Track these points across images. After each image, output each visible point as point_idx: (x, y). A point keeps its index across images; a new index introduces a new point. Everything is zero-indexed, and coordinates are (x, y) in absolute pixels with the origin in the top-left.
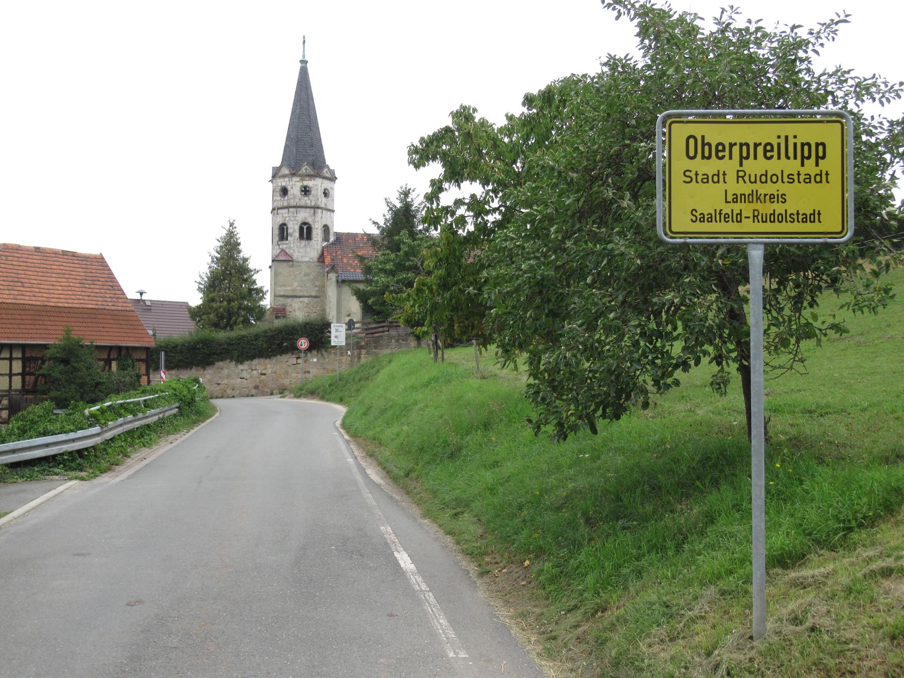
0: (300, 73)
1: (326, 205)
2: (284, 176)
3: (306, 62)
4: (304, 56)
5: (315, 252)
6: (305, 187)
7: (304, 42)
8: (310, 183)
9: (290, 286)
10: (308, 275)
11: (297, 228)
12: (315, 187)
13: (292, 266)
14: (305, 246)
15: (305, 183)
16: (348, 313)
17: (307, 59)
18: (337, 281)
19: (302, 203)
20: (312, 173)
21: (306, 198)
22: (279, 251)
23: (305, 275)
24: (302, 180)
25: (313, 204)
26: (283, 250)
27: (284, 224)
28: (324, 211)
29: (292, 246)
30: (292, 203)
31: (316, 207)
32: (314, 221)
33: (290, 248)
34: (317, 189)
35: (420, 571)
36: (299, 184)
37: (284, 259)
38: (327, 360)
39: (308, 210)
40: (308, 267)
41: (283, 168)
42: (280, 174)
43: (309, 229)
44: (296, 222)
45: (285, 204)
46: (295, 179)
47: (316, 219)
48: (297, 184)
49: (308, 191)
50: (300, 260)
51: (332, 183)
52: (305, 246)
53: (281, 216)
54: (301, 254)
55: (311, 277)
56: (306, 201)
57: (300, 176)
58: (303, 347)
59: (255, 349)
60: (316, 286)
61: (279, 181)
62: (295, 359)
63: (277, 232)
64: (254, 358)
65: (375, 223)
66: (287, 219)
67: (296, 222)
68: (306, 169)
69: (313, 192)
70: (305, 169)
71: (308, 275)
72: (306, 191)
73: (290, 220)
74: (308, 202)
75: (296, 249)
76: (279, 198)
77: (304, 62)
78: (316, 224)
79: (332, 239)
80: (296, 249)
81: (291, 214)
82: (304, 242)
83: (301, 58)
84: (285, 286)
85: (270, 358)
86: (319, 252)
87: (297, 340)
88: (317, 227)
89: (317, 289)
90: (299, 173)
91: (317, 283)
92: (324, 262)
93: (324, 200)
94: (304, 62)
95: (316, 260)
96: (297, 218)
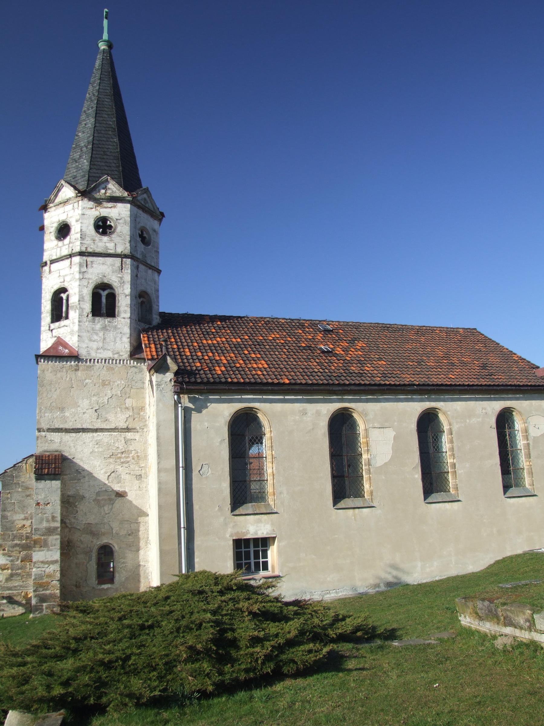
1: (144, 256)
6: (104, 220)
11: (87, 293)
14: (104, 328)
21: (105, 238)
27: (64, 290)
35: (106, 304)
39: (109, 260)
43: (112, 298)
49: (110, 227)
50: (93, 355)
65: (174, 575)
66: (67, 279)
82: (100, 322)
87: (461, 626)
94: (160, 225)
96: (86, 276)
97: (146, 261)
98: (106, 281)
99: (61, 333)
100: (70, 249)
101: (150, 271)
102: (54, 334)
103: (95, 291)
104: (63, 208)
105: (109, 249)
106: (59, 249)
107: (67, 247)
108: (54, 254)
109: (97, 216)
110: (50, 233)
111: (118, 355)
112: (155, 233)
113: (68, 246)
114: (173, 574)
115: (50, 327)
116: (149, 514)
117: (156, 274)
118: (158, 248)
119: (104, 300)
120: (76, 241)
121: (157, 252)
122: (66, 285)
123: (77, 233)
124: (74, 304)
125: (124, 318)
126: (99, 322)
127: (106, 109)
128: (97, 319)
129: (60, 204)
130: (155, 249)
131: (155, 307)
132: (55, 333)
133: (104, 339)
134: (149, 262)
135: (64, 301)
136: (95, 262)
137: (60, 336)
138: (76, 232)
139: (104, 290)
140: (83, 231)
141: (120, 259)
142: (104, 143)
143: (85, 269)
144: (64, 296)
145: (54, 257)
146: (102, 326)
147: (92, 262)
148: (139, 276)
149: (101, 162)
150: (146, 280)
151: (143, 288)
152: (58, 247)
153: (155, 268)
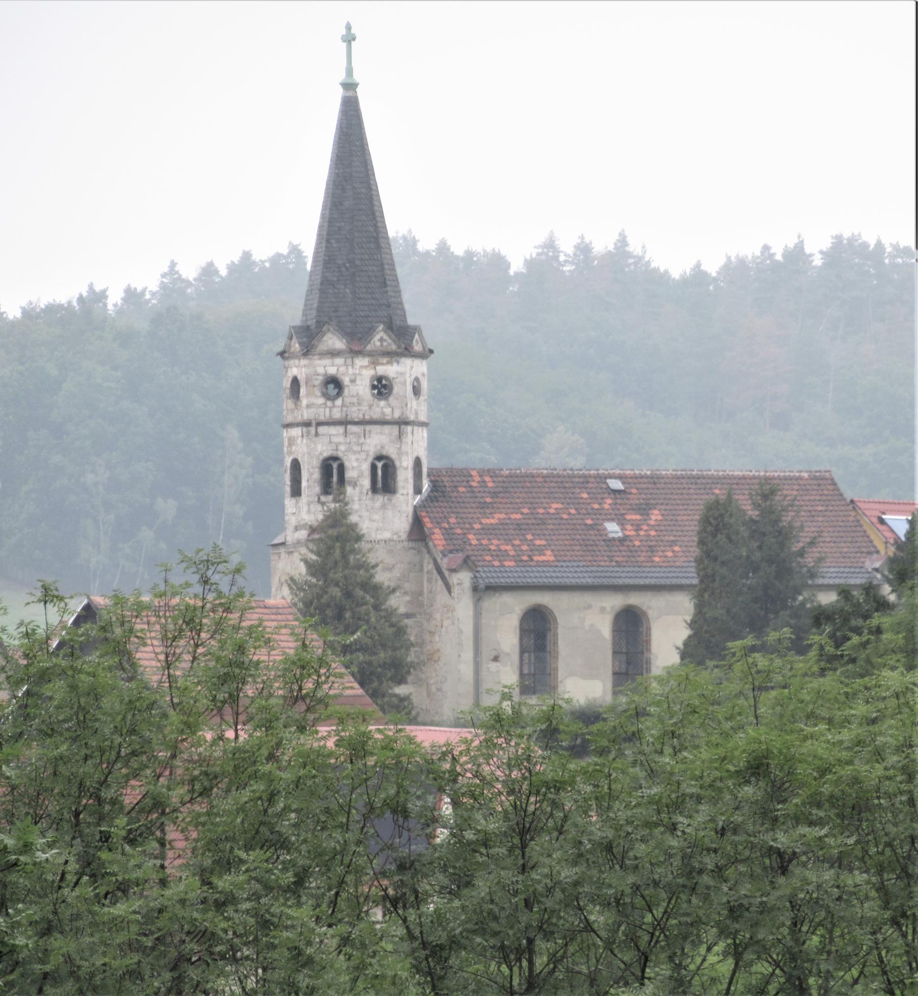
4: (349, 71)
6: (380, 379)
8: (389, 370)
11: (366, 467)
14: (384, 507)
15: (381, 370)
16: (494, 653)
18: (475, 589)
19: (376, 414)
21: (382, 403)
24: (374, 364)
25: (397, 415)
31: (402, 423)
32: (400, 453)
34: (405, 383)
36: (369, 373)
39: (387, 429)
40: (390, 551)
44: (363, 456)
45: (337, 414)
46: (361, 362)
47: (404, 448)
52: (384, 507)
54: (375, 525)
56: (382, 409)
57: (370, 354)
61: (318, 362)
66: (342, 448)
67: (363, 456)
68: (381, 340)
69: (396, 389)
70: (380, 338)
72: (382, 387)
74: (388, 411)
75: (365, 514)
77: (350, 86)
78: (404, 458)
80: (365, 514)
82: (380, 499)
88: (405, 464)
89: (407, 598)
90: (369, 348)
94: (350, 86)
95: (404, 536)
96: (365, 448)
98: (384, 453)
100: (344, 414)
106: (328, 410)
107: (339, 409)
108: (322, 414)
114: (446, 593)
115: (319, 499)
116: (357, 35)
122: (340, 454)
123: (353, 396)
133: (384, 518)
135: (335, 471)
141: (396, 428)
143: (362, 440)
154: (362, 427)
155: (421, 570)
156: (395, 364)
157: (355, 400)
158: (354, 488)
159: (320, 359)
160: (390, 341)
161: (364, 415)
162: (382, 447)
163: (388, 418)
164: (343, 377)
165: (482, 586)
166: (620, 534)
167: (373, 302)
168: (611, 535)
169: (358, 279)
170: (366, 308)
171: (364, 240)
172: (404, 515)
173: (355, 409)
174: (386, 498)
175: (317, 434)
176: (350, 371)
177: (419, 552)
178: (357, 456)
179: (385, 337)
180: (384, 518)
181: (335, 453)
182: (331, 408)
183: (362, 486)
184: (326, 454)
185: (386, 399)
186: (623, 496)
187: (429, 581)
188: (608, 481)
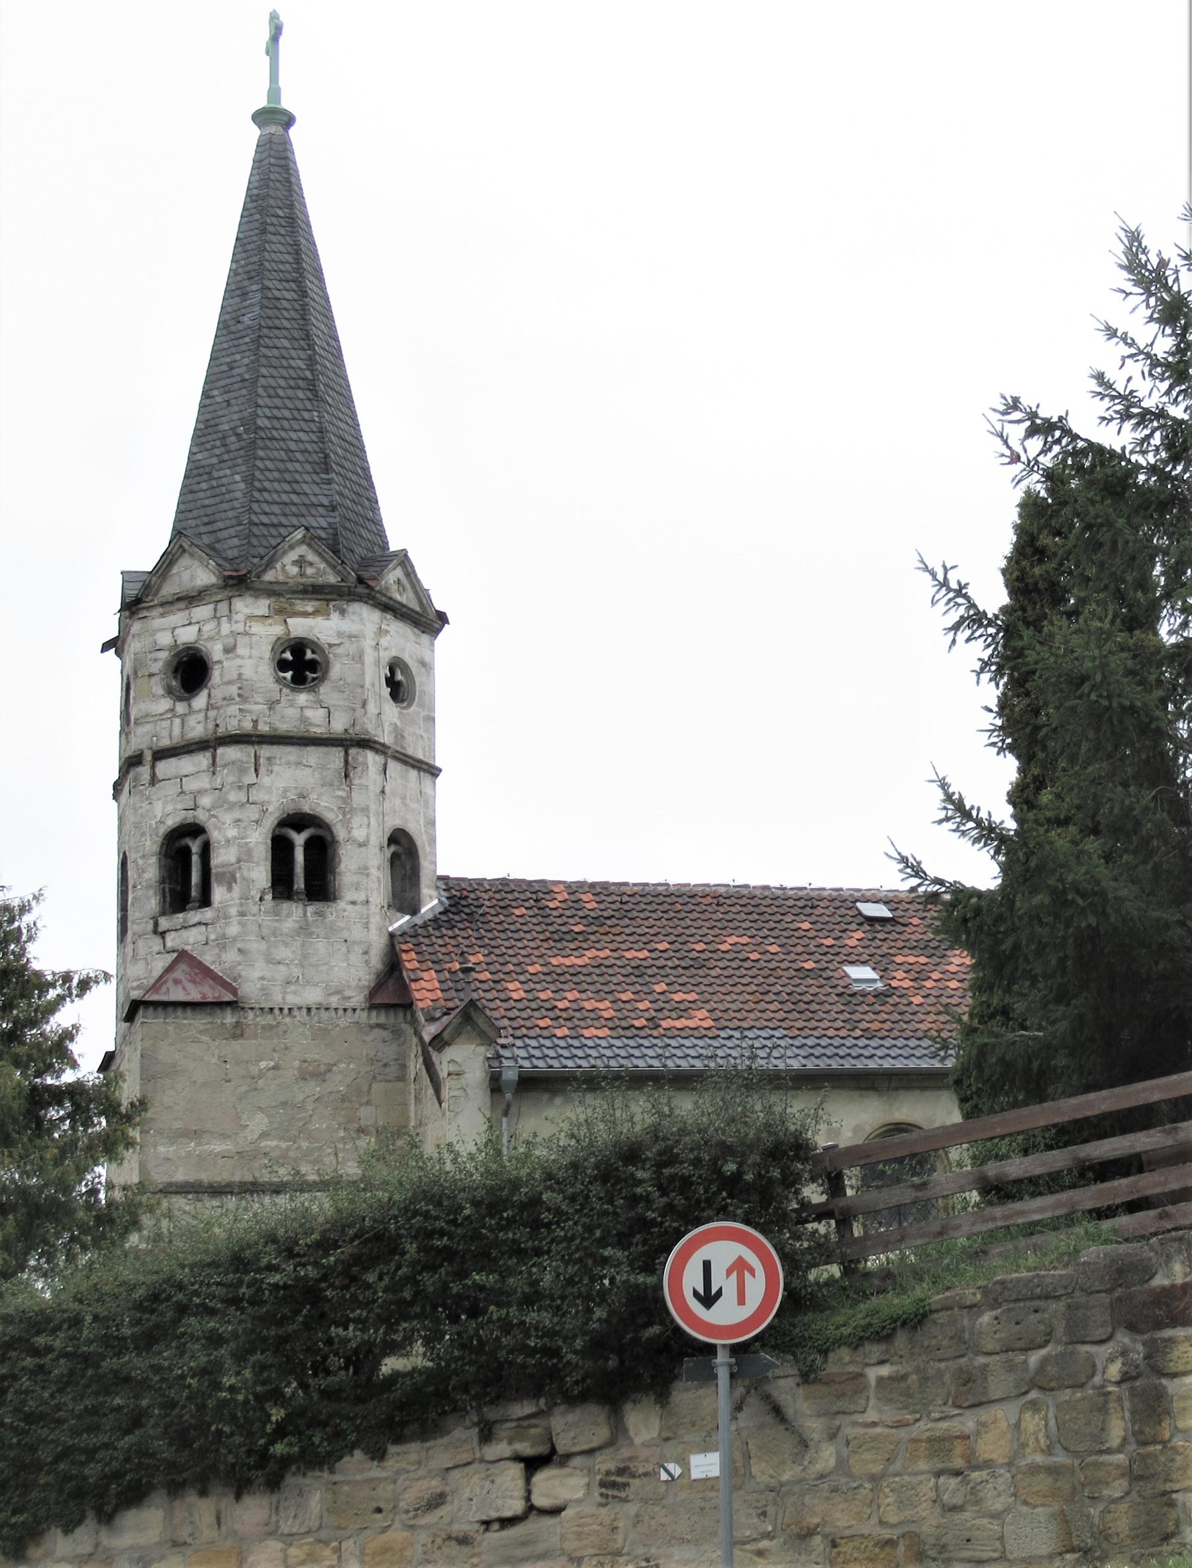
0: (258, 163)
1: (399, 735)
2: (191, 599)
3: (288, 120)
4: (274, 92)
5: (356, 958)
6: (298, 647)
7: (275, 37)
9: (224, 1136)
10: (320, 1075)
11: (259, 840)
12: (349, 648)
13: (238, 1032)
15: (299, 627)
17: (286, 104)
18: (495, 1085)
20: (332, 579)
21: (303, 698)
22: (160, 964)
23: (303, 1077)
24: (283, 613)
25: (339, 725)
26: (183, 956)
28: (394, 767)
29: (233, 930)
30: (232, 722)
32: (346, 808)
33: (223, 943)
34: (359, 657)
37: (195, 995)
38: (826, 1457)
39: (313, 755)
40: (322, 1034)
41: (185, 561)
42: (169, 589)
44: (252, 813)
45: (197, 729)
46: (245, 606)
47: (358, 798)
48: (257, 628)
49: (313, 665)
50: (277, 999)
51: (425, 638)
52: (304, 930)
53: (171, 789)
55: (337, 1083)
57: (272, 591)
58: (725, 1313)
59: (137, 1420)
60: (361, 1131)
61: (158, 623)
62: (515, 1471)
63: (149, 871)
64: (135, 1496)
66: (205, 801)
68: (301, 562)
69: (336, 670)
71: (320, 1075)
73: (218, 804)
74: (316, 716)
75: (255, 946)
76: (165, 704)
78: (357, 820)
79: (430, 904)
80: (255, 946)
81: (226, 776)
82: (294, 912)
83: (262, 102)
84: (197, 1134)
85: (274, 1484)
86: (376, 960)
88: (359, 834)
90: (269, 576)
91: (367, 1115)
92: (406, 1006)
93: (391, 710)
95: (358, 998)
96: (255, 795)
97: (403, 748)
98: (306, 808)
99: (191, 940)
100: (211, 726)
101: (413, 774)
102: (169, 944)
103: (277, 832)
104: (187, 612)
105: (311, 724)
106: (177, 721)
107: (201, 717)
108: (165, 733)
109: (279, 639)
110: (151, 675)
111: (338, 996)
112: (423, 670)
113: (203, 714)
115: (156, 924)
117: (427, 778)
118: (432, 708)
119: (299, 856)
120: (225, 703)
121: (432, 720)
122: (201, 817)
123: (229, 683)
124: (225, 869)
125: (354, 903)
126: (289, 915)
127: (286, 324)
128: (286, 906)
129: (179, 599)
130: (425, 713)
131: (424, 863)
132: (172, 940)
133: (305, 957)
134: (410, 752)
135: (195, 859)
136: (278, 762)
137: (188, 948)
138: (225, 680)
139: (299, 829)
140: (244, 677)
142: (286, 424)
143: (250, 778)
144: (195, 847)
145: (165, 742)
146: (297, 925)
147: (269, 759)
148: (387, 790)
149: (279, 481)
150: (404, 798)
151: (397, 823)
152: (175, 716)
153: (427, 764)
154: (251, 750)
155: (402, 1078)
156: (335, 616)
157: (233, 690)
158: (230, 889)
159: (162, 615)
160: (322, 566)
161: (255, 722)
162: (302, 796)
163: (318, 731)
164: (209, 645)
165: (510, 1075)
166: (879, 985)
167: (295, 498)
168: (856, 988)
169: (261, 453)
170: (276, 509)
171: (282, 383)
172: (359, 949)
173: (233, 709)
174: (310, 909)
175: (154, 780)
176: (226, 628)
177: (397, 1034)
178: (237, 814)
179: (311, 557)
180: (305, 957)
181: (189, 817)
182: (183, 717)
183: (248, 882)
184: (171, 822)
185: (313, 690)
186: (889, 928)
187: (418, 1099)
188: (858, 904)
